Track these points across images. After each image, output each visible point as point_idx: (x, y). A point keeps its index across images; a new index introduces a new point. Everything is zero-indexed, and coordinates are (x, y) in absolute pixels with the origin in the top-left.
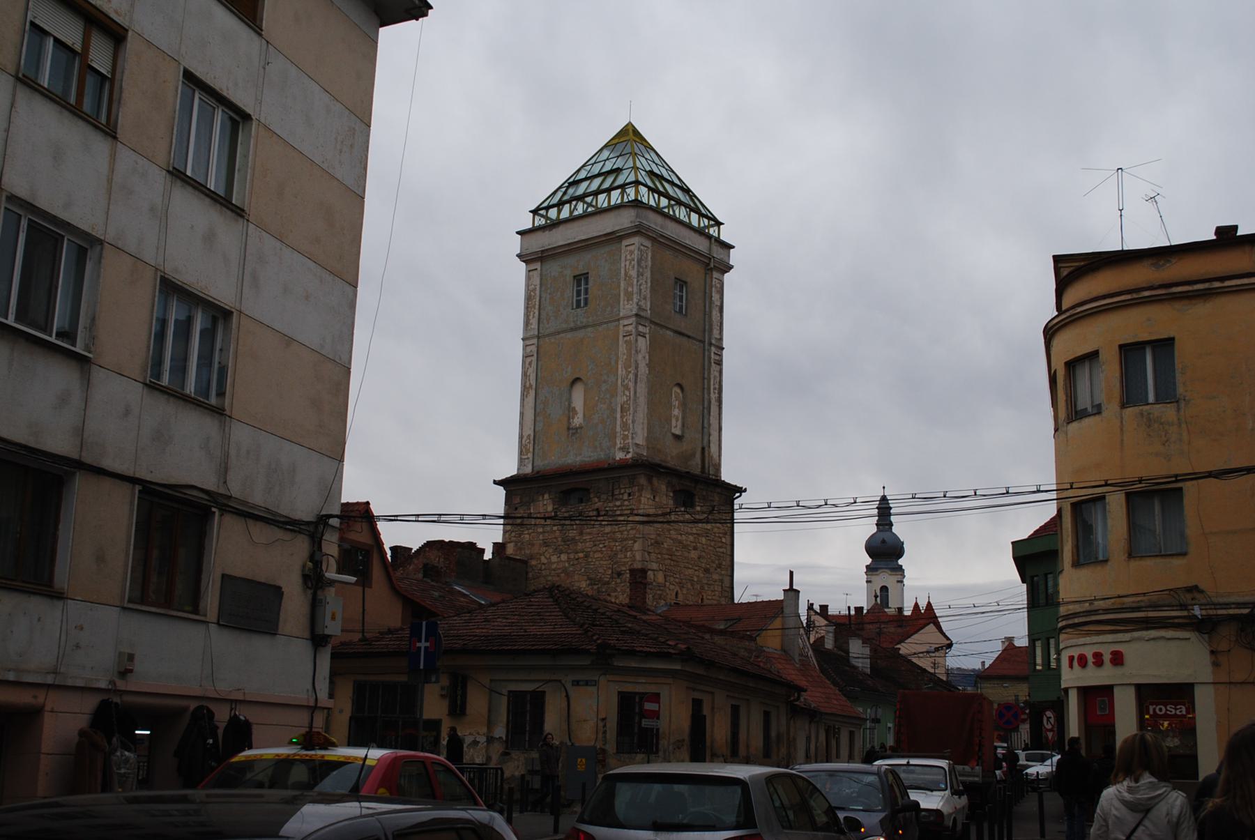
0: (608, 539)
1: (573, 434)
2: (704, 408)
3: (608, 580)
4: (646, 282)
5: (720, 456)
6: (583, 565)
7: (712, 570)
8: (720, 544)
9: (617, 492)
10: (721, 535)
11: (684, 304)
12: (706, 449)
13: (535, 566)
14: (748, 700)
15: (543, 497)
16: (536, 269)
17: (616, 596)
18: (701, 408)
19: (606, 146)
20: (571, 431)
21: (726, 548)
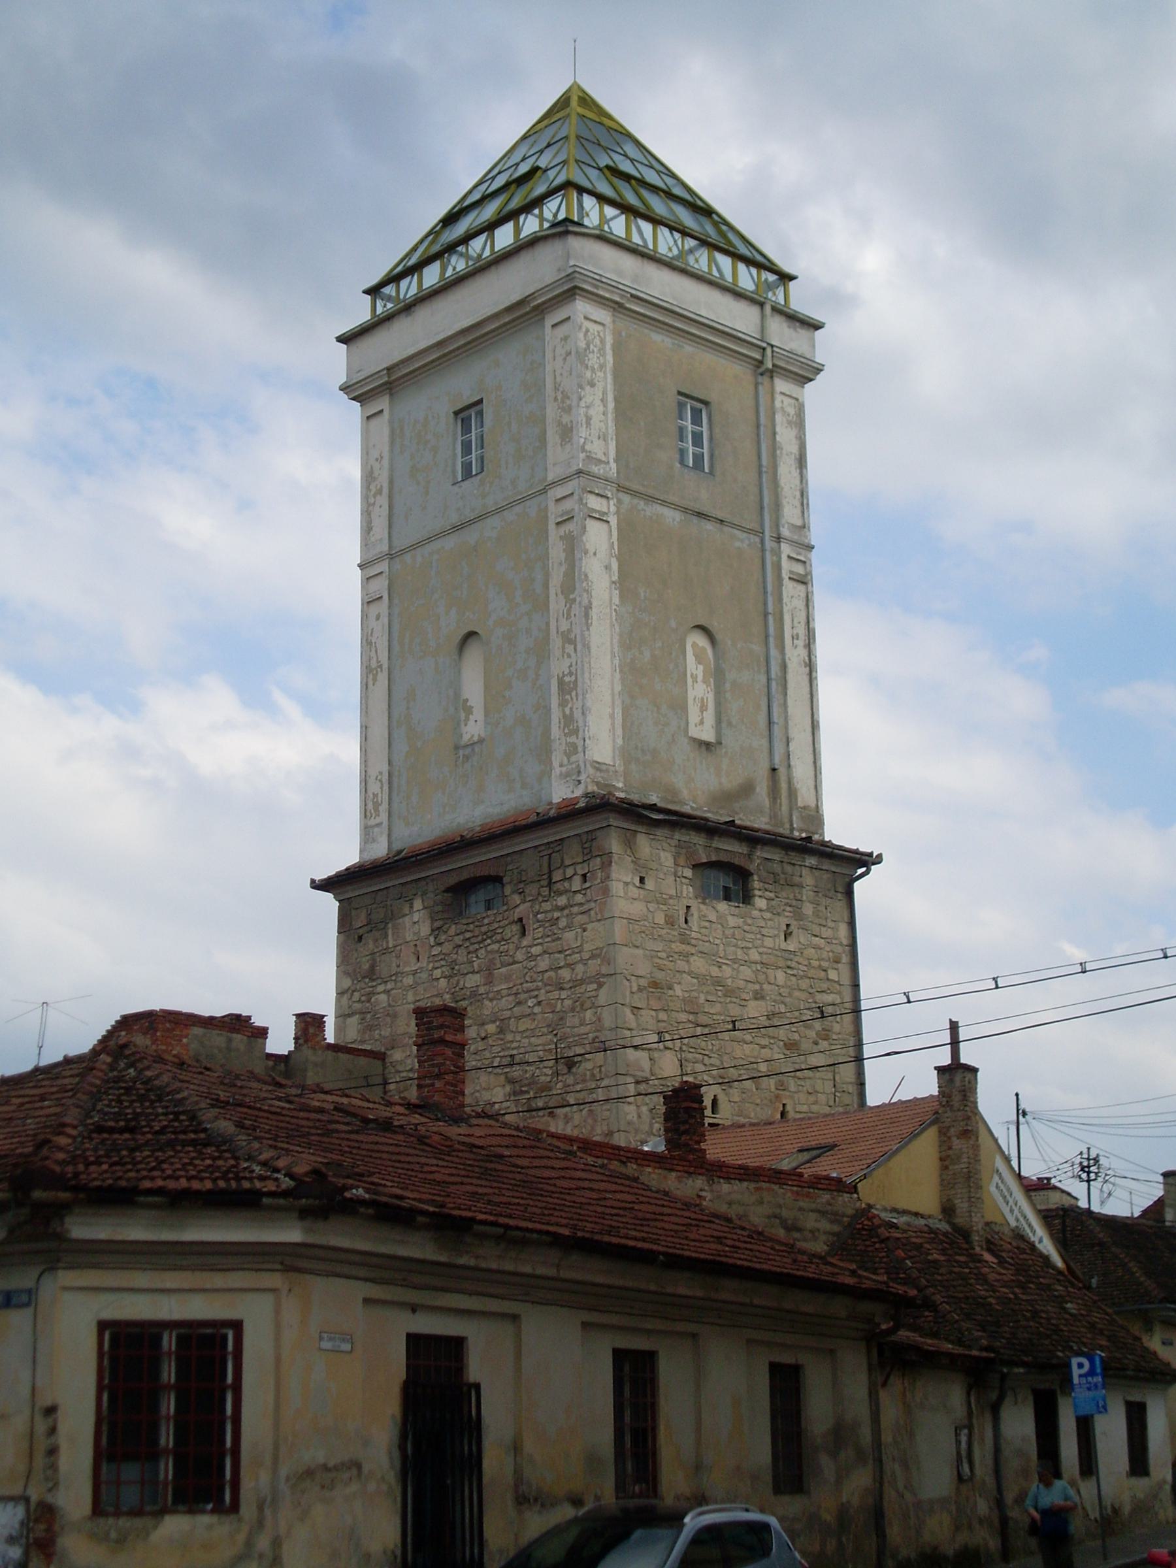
0: (546, 985)
1: (467, 758)
2: (769, 680)
3: (548, 1079)
4: (602, 400)
5: (817, 788)
6: (496, 1049)
7: (806, 1046)
8: (825, 986)
9: (557, 876)
10: (825, 964)
11: (706, 451)
12: (782, 772)
13: (401, 1062)
14: (694, 1336)
15: (411, 907)
16: (381, 411)
17: (566, 1116)
18: (764, 679)
19: (524, 138)
20: (461, 752)
21: (839, 993)
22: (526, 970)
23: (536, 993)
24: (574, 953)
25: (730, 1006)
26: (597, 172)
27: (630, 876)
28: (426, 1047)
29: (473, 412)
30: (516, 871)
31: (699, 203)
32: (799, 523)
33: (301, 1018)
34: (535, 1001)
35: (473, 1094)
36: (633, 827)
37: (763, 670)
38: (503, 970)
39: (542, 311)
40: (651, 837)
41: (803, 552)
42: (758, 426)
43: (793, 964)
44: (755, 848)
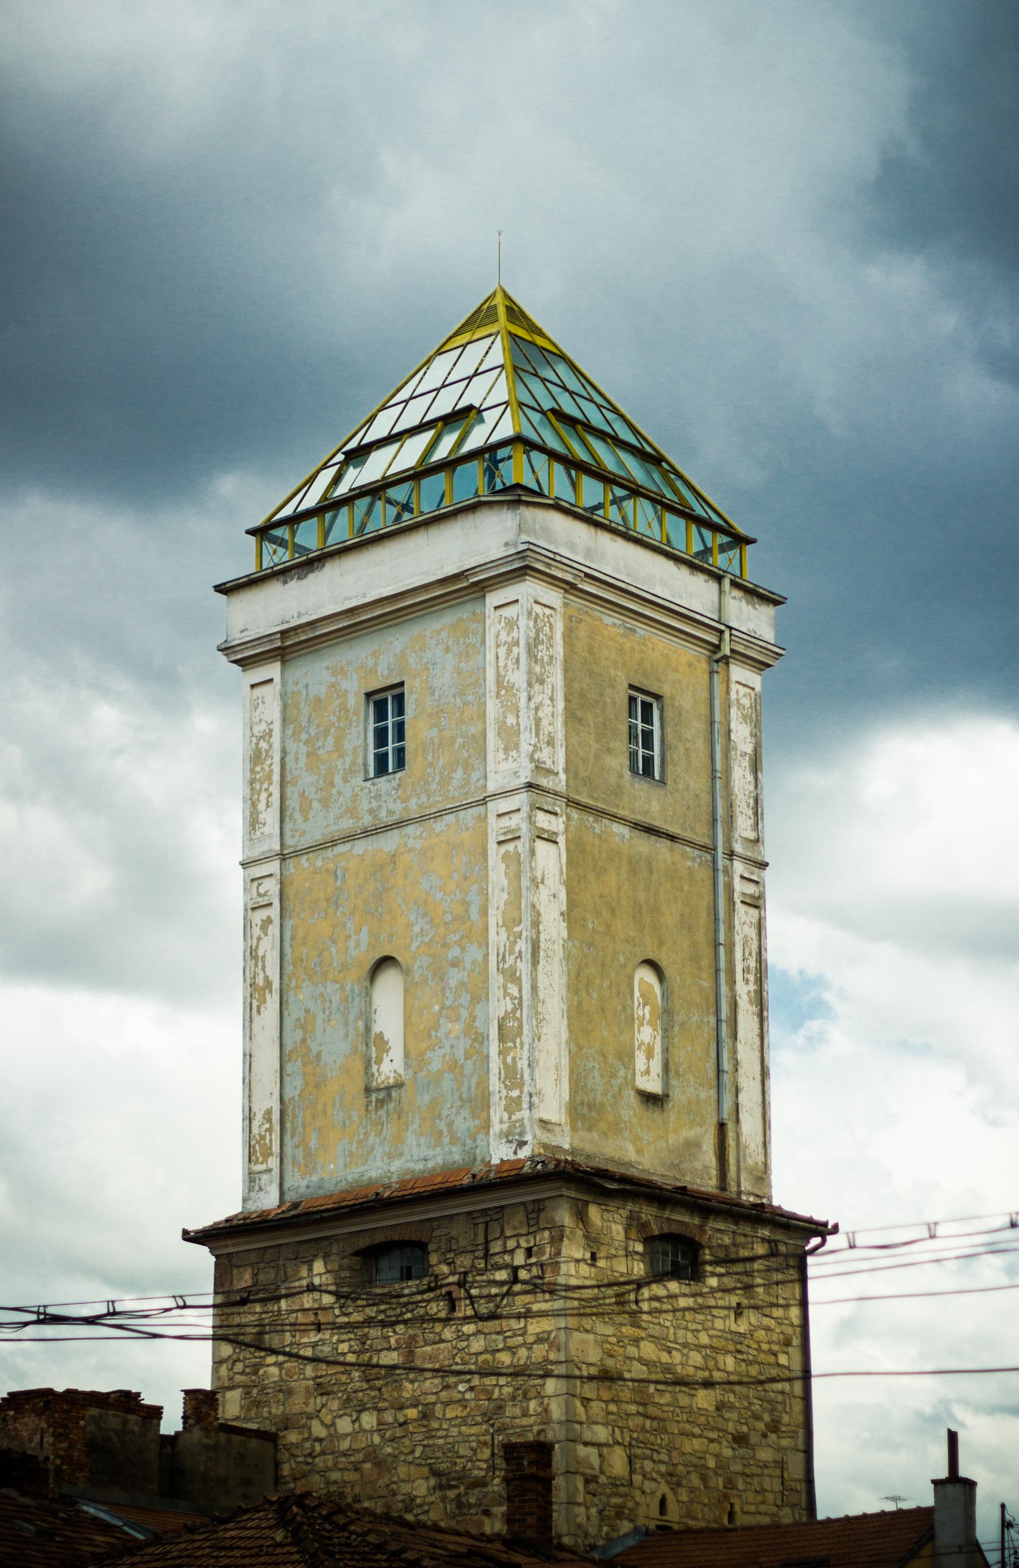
1: (381, 1103)
2: (718, 1021)
3: (482, 1473)
7: (754, 1438)
9: (496, 1247)
10: (775, 1348)
12: (730, 1126)
13: (297, 1446)
15: (310, 1269)
16: (271, 680)
18: (713, 1020)
22: (456, 1351)
23: (468, 1377)
24: (515, 1335)
25: (680, 1396)
26: (539, 415)
27: (582, 1251)
28: (517, 1482)
29: (389, 696)
30: (444, 1239)
31: (648, 449)
32: (752, 835)
33: (191, 1396)
34: (466, 1386)
35: (388, 1486)
36: (585, 1197)
37: (713, 1010)
38: (428, 1349)
39: (483, 589)
40: (603, 1207)
41: (756, 870)
42: (712, 723)
43: (744, 1348)
44: (708, 1219)
